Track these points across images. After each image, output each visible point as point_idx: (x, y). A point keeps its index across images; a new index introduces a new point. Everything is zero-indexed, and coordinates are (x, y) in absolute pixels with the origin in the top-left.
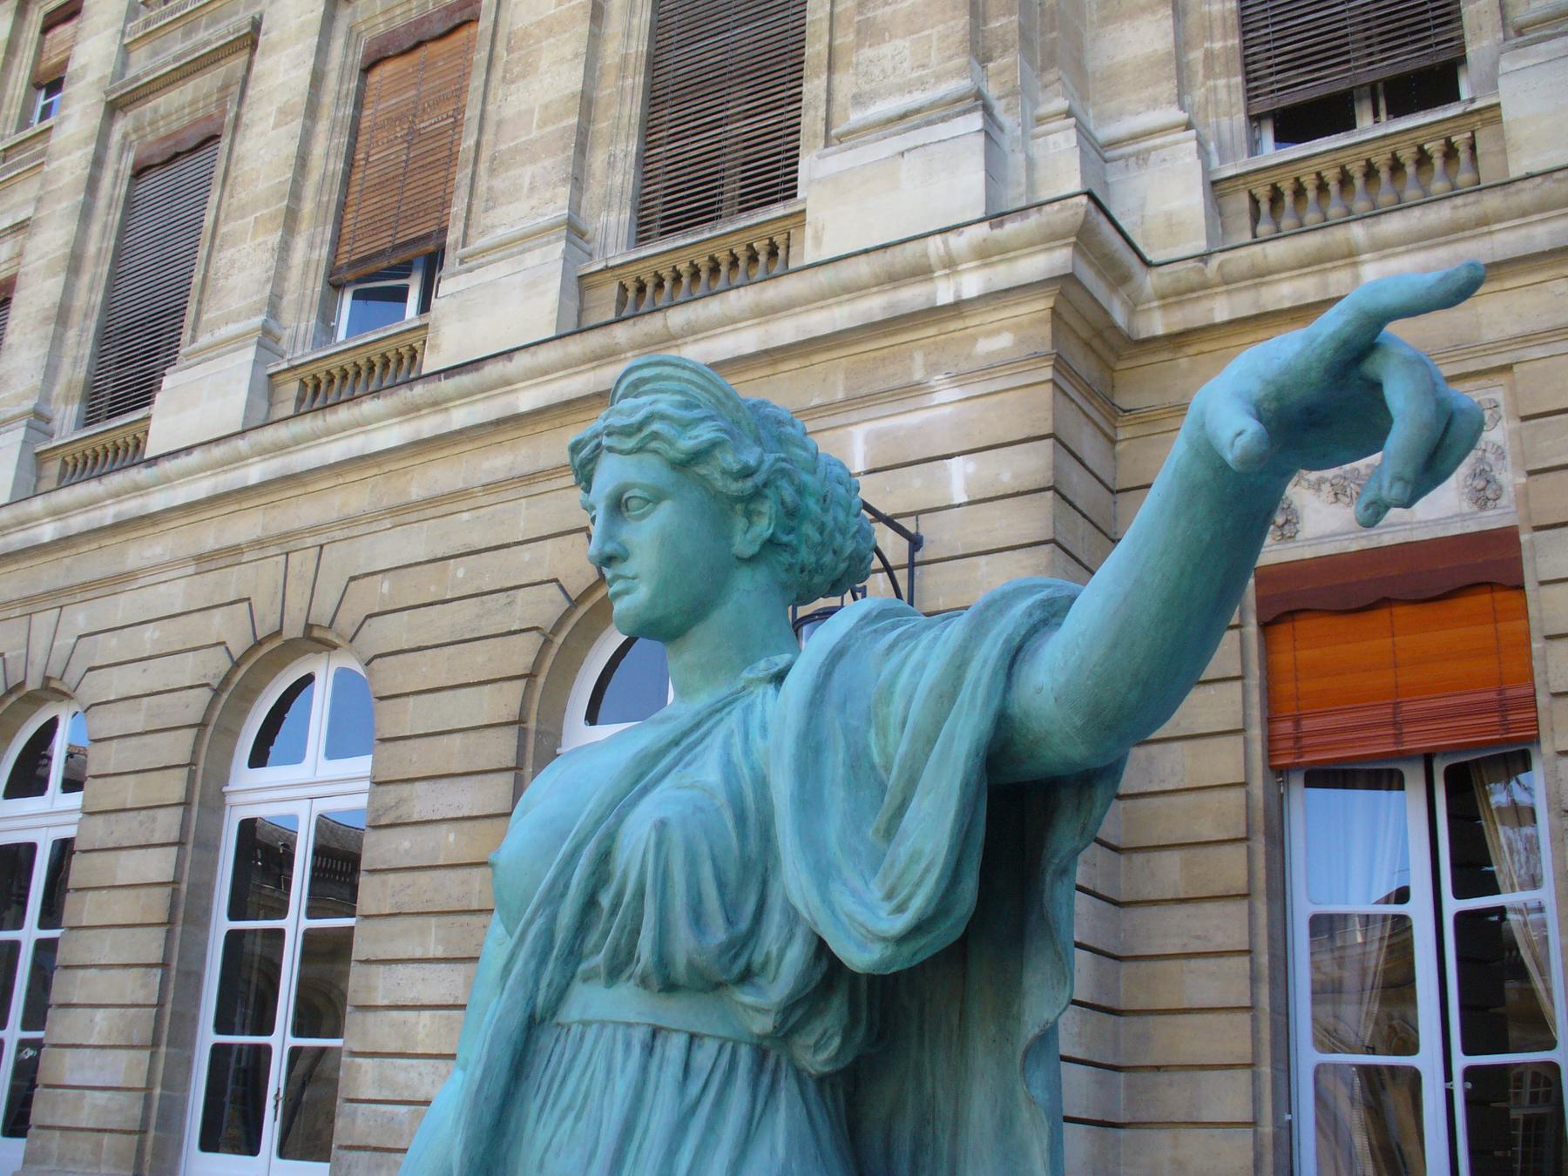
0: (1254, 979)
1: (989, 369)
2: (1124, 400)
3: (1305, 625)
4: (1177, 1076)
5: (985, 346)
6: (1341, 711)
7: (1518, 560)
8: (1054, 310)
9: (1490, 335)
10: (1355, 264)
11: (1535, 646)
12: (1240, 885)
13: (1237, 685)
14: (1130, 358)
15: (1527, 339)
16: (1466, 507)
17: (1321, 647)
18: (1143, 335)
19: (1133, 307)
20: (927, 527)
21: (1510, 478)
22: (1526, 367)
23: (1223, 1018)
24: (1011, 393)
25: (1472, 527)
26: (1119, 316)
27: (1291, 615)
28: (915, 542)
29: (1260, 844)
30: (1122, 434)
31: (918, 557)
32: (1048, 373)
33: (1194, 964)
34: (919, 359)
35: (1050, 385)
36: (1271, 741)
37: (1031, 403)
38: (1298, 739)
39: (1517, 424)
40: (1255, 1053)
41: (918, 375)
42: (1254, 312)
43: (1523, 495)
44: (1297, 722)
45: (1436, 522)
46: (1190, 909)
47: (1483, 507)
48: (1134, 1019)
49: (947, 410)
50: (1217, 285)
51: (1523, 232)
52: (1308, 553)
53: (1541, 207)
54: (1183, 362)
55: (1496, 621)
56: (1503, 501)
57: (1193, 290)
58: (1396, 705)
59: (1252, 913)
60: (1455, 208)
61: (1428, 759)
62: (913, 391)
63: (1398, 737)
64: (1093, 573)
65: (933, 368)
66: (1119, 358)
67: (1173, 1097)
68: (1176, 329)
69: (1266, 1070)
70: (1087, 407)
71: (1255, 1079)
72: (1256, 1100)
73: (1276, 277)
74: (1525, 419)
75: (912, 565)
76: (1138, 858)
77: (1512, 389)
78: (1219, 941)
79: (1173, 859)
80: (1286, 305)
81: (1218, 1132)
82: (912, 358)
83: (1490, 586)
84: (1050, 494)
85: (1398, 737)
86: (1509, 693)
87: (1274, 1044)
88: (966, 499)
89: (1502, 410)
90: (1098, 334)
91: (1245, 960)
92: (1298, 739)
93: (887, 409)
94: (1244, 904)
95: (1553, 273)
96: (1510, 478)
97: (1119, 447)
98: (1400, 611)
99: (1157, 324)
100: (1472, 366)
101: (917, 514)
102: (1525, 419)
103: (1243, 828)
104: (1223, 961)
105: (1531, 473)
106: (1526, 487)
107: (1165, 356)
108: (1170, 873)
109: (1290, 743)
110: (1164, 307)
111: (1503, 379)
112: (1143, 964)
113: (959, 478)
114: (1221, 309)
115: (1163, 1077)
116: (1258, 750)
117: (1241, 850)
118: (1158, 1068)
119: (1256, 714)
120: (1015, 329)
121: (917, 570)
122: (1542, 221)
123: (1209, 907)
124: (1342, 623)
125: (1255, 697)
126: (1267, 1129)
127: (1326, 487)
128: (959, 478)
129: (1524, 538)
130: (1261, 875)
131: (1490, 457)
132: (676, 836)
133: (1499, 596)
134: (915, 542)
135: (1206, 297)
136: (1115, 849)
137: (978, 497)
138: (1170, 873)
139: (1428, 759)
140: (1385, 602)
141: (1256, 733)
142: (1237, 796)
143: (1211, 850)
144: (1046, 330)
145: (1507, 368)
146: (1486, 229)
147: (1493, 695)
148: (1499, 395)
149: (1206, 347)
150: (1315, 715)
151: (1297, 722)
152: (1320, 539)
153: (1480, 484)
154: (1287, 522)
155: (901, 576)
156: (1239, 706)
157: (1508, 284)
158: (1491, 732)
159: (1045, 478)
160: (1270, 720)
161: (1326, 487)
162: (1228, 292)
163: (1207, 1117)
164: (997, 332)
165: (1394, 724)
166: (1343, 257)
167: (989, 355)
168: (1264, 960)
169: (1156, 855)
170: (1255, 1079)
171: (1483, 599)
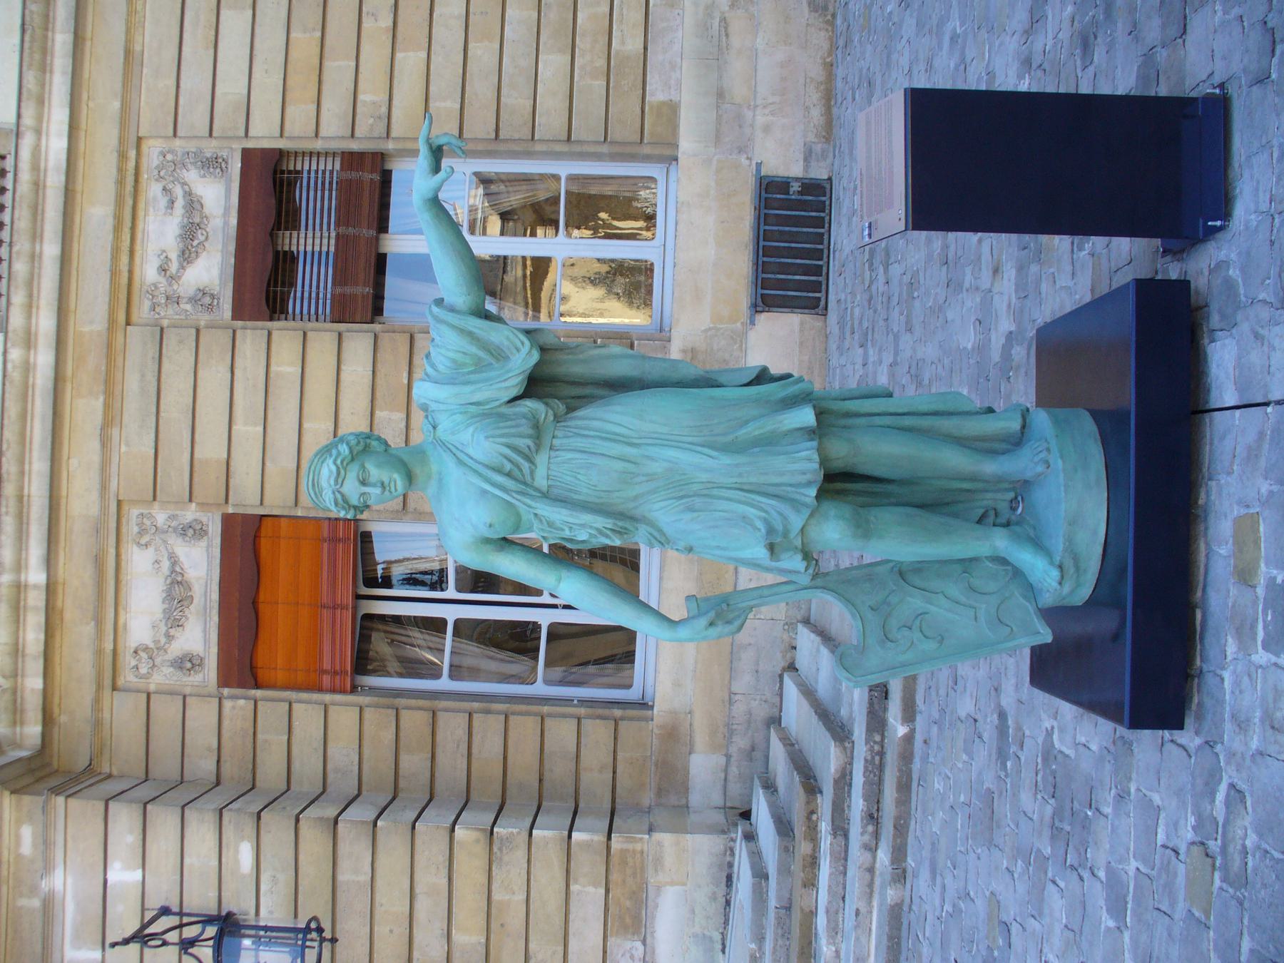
0: (488, 712)
1: (45, 843)
2: (82, 763)
3: (262, 658)
4: (547, 766)
5: (27, 848)
6: (321, 642)
7: (245, 516)
8: (12, 792)
9: (95, 510)
10: (26, 586)
11: (299, 514)
12: (426, 716)
13: (295, 706)
14: (51, 757)
15: (104, 487)
16: (203, 543)
17: (276, 650)
18: (39, 741)
19: (16, 745)
20: (154, 903)
21: (190, 514)
22: (121, 491)
23: (511, 733)
24: (69, 830)
25: (217, 541)
26: (24, 754)
27: (253, 669)
28: (165, 911)
29: (402, 702)
30: (106, 769)
31: (175, 909)
32: (60, 800)
33: (475, 751)
34: (23, 902)
35: (70, 800)
36: (333, 691)
37: (78, 814)
38: (335, 673)
39: (156, 504)
40: (536, 714)
41: (36, 903)
42: (41, 661)
43: (203, 506)
44: (324, 672)
45: (209, 564)
46: (439, 751)
47: (206, 533)
48: (508, 793)
49: (70, 881)
50: (16, 682)
51: (34, 477)
52: (214, 650)
53: (21, 461)
54: (63, 719)
55: (279, 537)
56: (204, 520)
57: (15, 701)
58: (323, 606)
59: (446, 710)
60: (7, 513)
61: (359, 597)
62: (49, 906)
63: (343, 607)
64: (505, 258)
65: (34, 890)
66: (49, 764)
67: (559, 770)
68: (40, 717)
69: (546, 709)
70: (82, 786)
71: (550, 715)
72: (564, 716)
73: (21, 640)
74: (155, 499)
75: (181, 914)
76: (402, 784)
77: (134, 502)
78: (461, 733)
79: (405, 759)
80: (42, 636)
81: (583, 740)
82: (21, 908)
83: (257, 537)
84: (149, 807)
85: (343, 607)
86: (326, 534)
87: (528, 704)
88: (140, 871)
89: (145, 512)
90: (32, 771)
91: (475, 716)
92: (335, 673)
93: (57, 929)
94: (439, 714)
95: (64, 465)
96: (190, 514)
97: (115, 772)
98: (262, 597)
99: (33, 730)
100: (113, 525)
101: (143, 910)
102: (155, 499)
103: (390, 711)
104: (475, 731)
105: (191, 500)
106: (198, 504)
107: (56, 730)
108: (414, 763)
109: (338, 677)
110: (22, 723)
111: (125, 508)
112: (473, 785)
113: (123, 875)
114: (34, 682)
115: (547, 776)
116: (339, 697)
117: (403, 713)
118: (541, 780)
119: (316, 696)
120: (19, 823)
121: (185, 911)
122: (30, 463)
123: (439, 738)
124: (263, 635)
125: (304, 696)
126: (582, 711)
127: (172, 632)
128: (123, 875)
129: (231, 510)
130: (421, 703)
131: (174, 524)
132: (490, 433)
133: (263, 533)
134: (165, 911)
135: (23, 691)
136: (394, 799)
137: (141, 862)
138: (414, 763)
139: (359, 597)
140: (255, 603)
141: (328, 697)
142: (368, 714)
143: (401, 734)
144: (27, 799)
145: (119, 503)
146: (25, 499)
147: (326, 545)
148: (135, 512)
149: (56, 700)
150: (321, 659)
151: (324, 672)
152: (206, 641)
153: (191, 532)
154: (190, 661)
155: (185, 920)
156: (309, 706)
157: (64, 493)
158: (349, 548)
159: (136, 811)
160: (320, 690)
161: (172, 632)
162: (23, 676)
163: (572, 748)
164: (18, 838)
165: (334, 608)
166: (19, 592)
167: (34, 845)
168: (476, 705)
169: (401, 772)
170: (550, 715)
171: (265, 544)
